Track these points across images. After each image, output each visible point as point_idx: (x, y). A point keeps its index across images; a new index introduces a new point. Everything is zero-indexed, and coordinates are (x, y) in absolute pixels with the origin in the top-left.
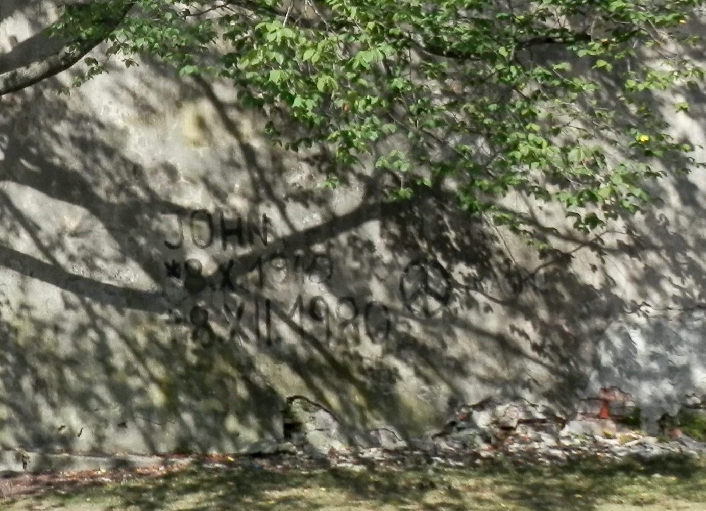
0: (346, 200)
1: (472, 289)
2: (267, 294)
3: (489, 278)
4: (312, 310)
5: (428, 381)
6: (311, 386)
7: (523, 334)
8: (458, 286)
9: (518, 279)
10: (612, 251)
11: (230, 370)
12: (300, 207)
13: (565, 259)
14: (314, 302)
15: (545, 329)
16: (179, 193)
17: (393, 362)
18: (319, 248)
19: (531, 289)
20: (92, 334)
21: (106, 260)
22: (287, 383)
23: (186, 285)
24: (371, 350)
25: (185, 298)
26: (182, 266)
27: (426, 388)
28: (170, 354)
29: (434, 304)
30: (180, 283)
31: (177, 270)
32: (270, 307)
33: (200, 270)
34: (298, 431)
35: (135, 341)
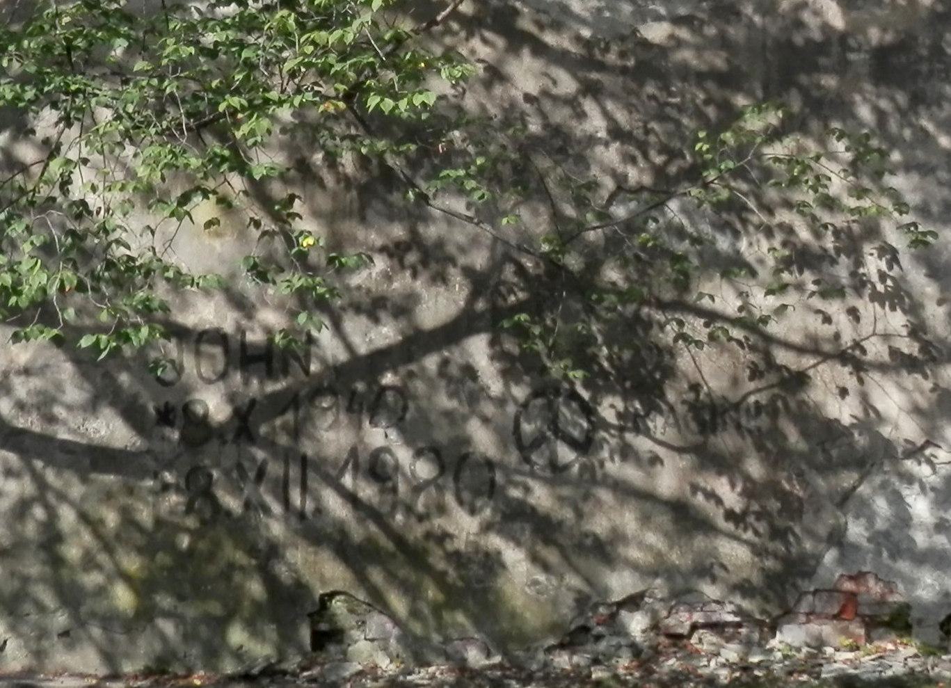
0: (438, 305)
1: (630, 430)
2: (308, 448)
3: (661, 412)
4: (377, 469)
5: (546, 567)
6: (362, 579)
7: (712, 496)
8: (606, 426)
9: (708, 415)
10: (882, 368)
11: (240, 557)
12: (363, 320)
13: (800, 380)
14: (377, 455)
15: (751, 491)
16: (185, 305)
17: (495, 541)
18: (388, 379)
19: (731, 428)
20: (39, 512)
21: (70, 408)
22: (326, 572)
23: (183, 437)
24: (464, 526)
25: (178, 456)
26: (180, 409)
27: (541, 577)
28: (155, 540)
29: (566, 454)
30: (176, 435)
31: (171, 417)
32: (311, 468)
33: (206, 416)
34: (340, 642)
35: (102, 522)
